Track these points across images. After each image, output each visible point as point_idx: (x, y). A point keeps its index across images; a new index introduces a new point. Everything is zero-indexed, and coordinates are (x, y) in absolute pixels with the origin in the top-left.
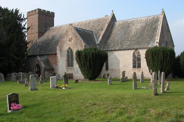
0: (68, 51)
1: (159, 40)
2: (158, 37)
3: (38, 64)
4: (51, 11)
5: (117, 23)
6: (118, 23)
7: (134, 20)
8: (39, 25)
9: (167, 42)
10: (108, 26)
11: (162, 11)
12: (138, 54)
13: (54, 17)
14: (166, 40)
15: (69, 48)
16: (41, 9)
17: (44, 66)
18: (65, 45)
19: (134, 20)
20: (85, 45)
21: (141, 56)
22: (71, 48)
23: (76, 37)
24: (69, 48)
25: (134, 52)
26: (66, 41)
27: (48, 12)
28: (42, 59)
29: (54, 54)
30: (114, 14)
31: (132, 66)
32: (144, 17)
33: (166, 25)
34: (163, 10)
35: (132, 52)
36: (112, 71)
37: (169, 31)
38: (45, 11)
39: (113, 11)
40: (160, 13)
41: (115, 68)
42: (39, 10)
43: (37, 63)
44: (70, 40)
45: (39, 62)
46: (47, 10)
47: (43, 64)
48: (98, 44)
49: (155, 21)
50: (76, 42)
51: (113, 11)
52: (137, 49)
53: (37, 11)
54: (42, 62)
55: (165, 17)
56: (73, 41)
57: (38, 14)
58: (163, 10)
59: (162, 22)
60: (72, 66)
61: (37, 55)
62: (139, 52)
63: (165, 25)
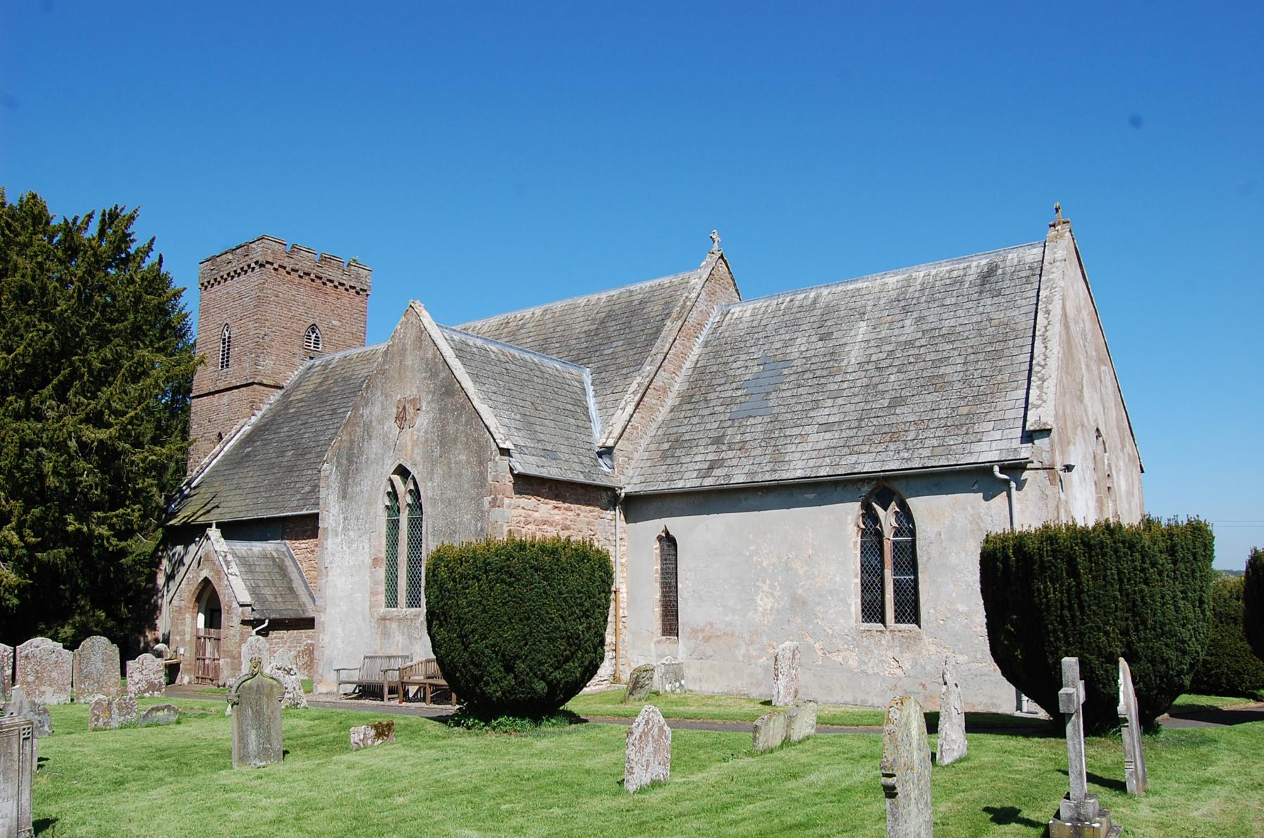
15: (403, 472)
26: (381, 421)
35: (851, 512)
36: (707, 639)
52: (882, 490)
54: (234, 569)
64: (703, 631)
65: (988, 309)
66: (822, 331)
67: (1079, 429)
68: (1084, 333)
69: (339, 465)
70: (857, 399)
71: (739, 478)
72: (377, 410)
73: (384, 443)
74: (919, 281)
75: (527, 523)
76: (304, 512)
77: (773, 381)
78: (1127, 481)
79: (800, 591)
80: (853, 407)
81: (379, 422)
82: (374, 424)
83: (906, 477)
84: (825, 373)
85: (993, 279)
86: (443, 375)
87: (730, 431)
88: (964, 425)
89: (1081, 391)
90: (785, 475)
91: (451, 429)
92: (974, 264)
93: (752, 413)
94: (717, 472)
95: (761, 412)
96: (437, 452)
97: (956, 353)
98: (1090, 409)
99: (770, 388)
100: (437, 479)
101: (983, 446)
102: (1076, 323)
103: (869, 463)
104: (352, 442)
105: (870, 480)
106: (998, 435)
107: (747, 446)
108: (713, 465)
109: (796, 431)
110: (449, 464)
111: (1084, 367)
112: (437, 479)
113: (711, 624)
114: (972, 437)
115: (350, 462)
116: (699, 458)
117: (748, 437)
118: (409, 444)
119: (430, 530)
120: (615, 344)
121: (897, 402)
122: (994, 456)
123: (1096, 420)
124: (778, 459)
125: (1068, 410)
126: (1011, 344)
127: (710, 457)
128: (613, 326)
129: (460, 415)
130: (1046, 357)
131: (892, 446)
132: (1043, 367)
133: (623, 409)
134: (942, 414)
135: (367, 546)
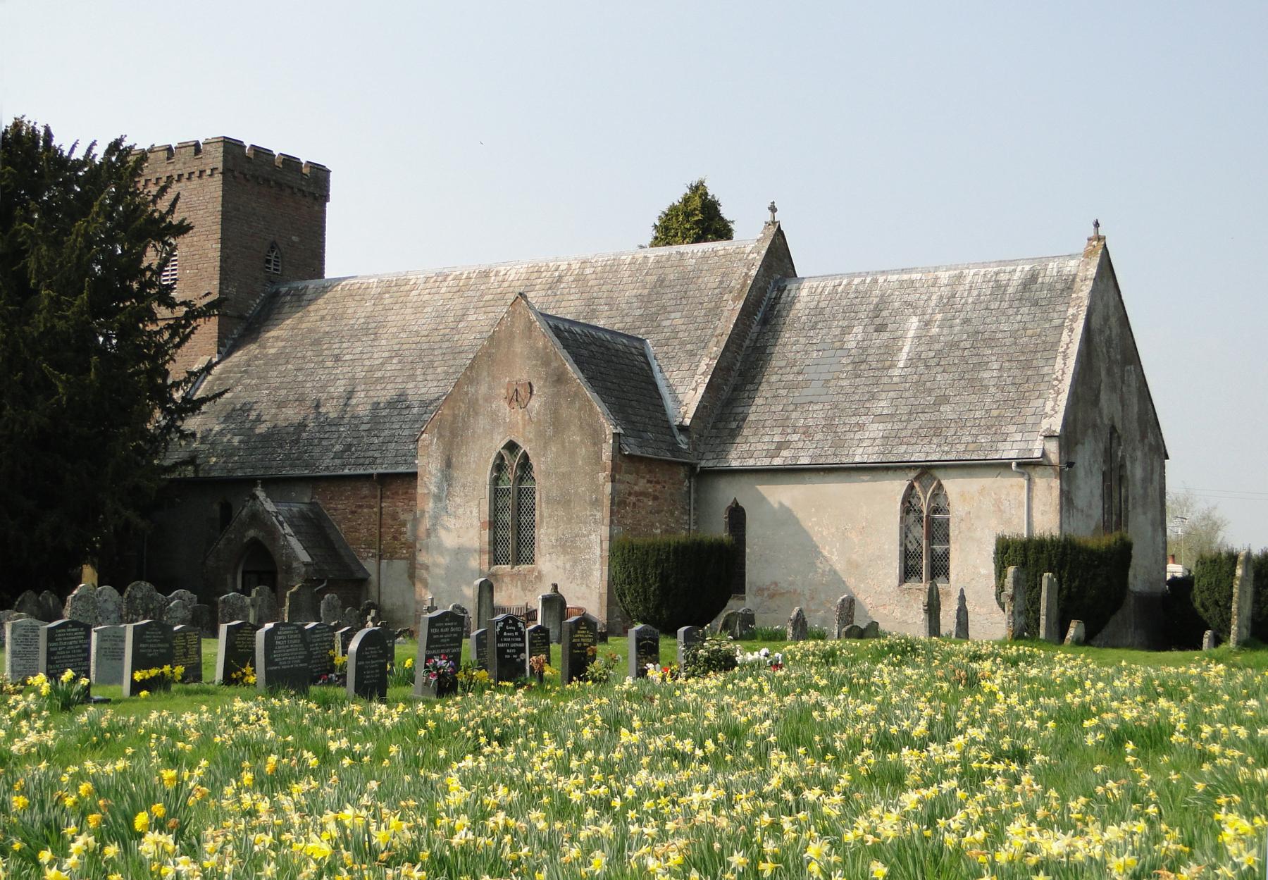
0: (499, 466)
1: (1060, 422)
2: (1055, 400)
3: (255, 542)
4: (305, 156)
5: (804, 296)
6: (806, 286)
7: (919, 276)
8: (224, 260)
9: (1113, 429)
10: (747, 313)
11: (1091, 232)
12: (934, 496)
13: (325, 198)
14: (1106, 421)
15: (512, 447)
16: (239, 145)
17: (304, 557)
18: (482, 422)
19: (914, 276)
20: (616, 436)
21: (951, 509)
22: (525, 447)
23: (560, 379)
24: (512, 447)
25: (911, 487)
26: (488, 399)
27: (291, 163)
28: (284, 508)
29: (371, 475)
30: (780, 233)
31: (894, 568)
32: (976, 265)
33: (1113, 321)
34: (1097, 224)
35: (896, 487)
36: (772, 596)
37: (1130, 355)
38: (268, 153)
39: (773, 209)
40: (1082, 245)
41: (791, 583)
42: (231, 147)
43: (251, 533)
44: (514, 398)
45: (272, 533)
46: (279, 147)
47: (295, 543)
48: (682, 429)
49: (1036, 292)
50: (555, 414)
51: (773, 209)
52: (925, 471)
53: (216, 158)
54: (288, 529)
55: (1106, 269)
56: (535, 404)
57: (218, 178)
58: (1097, 224)
59: (1084, 309)
60: (518, 561)
61: (250, 482)
62: (940, 486)
63: (1106, 319)
64: (768, 589)
65: (1026, 318)
66: (878, 321)
67: (1090, 431)
68: (1109, 341)
69: (441, 436)
70: (907, 394)
71: (804, 461)
72: (483, 389)
73: (493, 420)
74: (969, 279)
75: (630, 494)
76: (346, 471)
77: (833, 368)
78: (1144, 469)
79: (854, 557)
80: (904, 402)
81: (486, 400)
82: (481, 402)
83: (945, 467)
84: (879, 366)
85: (1034, 287)
86: (554, 364)
87: (794, 415)
88: (994, 427)
89: (1097, 396)
90: (844, 460)
91: (564, 412)
92: (1020, 268)
93: (814, 399)
94: (785, 453)
95: (822, 398)
96: (550, 432)
97: (994, 358)
98: (1105, 412)
99: (829, 376)
100: (550, 456)
101: (1007, 445)
102: (1101, 331)
103: (918, 454)
104: (455, 416)
105: (916, 467)
106: (1018, 437)
107: (811, 431)
108: (780, 446)
109: (854, 420)
110: (563, 443)
111: (1103, 373)
112: (550, 456)
113: (776, 584)
114: (999, 437)
115: (454, 434)
116: (766, 439)
117: (810, 422)
118: (521, 423)
119: (544, 499)
120: (673, 316)
121: (944, 400)
122: (1013, 454)
123: (1112, 419)
124: (839, 444)
125: (1080, 415)
126: (1039, 355)
127: (777, 439)
128: (668, 296)
129: (573, 402)
130: (1064, 373)
131: (935, 440)
132: (1060, 381)
133: (695, 389)
134: (978, 414)
135: (475, 511)
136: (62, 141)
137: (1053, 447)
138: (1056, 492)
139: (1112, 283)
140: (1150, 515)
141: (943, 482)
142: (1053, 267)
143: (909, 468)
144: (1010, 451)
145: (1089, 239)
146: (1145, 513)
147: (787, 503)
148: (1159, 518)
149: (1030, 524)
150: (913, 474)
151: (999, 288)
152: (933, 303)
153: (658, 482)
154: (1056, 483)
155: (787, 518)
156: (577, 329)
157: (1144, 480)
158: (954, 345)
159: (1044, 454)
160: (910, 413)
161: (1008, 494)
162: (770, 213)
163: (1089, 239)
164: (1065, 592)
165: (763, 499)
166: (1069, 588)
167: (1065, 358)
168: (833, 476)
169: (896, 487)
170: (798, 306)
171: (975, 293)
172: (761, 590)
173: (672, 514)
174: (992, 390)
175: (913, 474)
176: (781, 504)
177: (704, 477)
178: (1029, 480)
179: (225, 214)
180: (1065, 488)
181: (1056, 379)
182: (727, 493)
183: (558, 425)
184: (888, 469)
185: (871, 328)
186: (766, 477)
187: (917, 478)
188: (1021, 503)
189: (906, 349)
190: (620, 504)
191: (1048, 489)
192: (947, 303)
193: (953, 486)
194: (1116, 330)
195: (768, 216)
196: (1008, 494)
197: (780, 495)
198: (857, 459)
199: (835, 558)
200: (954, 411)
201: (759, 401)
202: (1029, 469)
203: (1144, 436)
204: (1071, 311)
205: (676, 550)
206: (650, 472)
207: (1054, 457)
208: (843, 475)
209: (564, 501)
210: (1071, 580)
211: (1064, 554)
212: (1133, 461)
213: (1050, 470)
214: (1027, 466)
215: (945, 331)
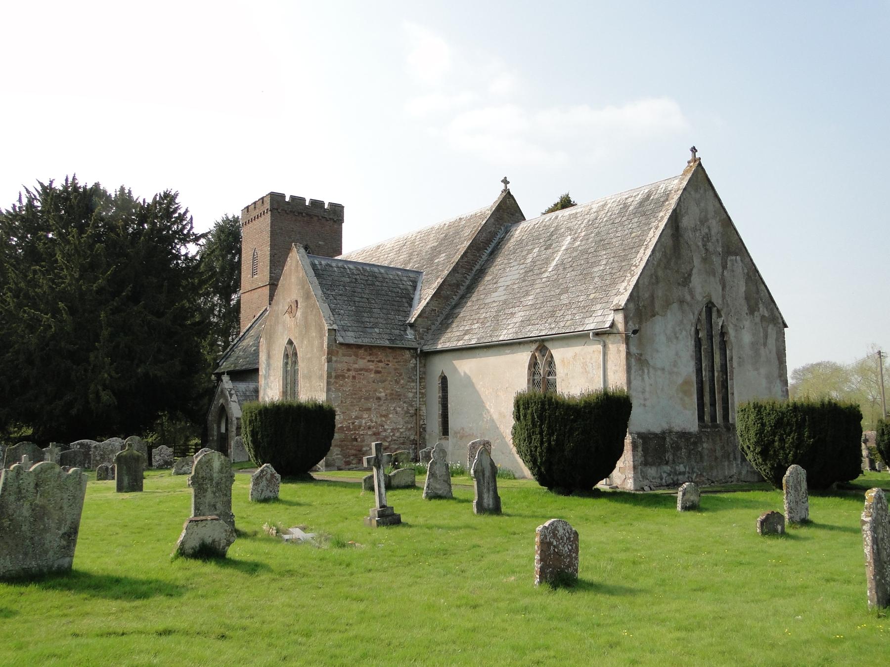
18: (280, 328)
25: (534, 357)
34: (694, 150)
38: (321, 204)
39: (505, 181)
42: (276, 198)
46: (309, 196)
52: (542, 345)
57: (269, 213)
75: (349, 370)
90: (494, 339)
103: (534, 332)
105: (536, 341)
121: (566, 290)
122: (592, 327)
136: (135, 196)
137: (620, 318)
138: (623, 354)
139: (711, 193)
140: (763, 371)
141: (552, 351)
142: (663, 186)
143: (531, 342)
144: (591, 325)
145: (689, 162)
146: (757, 369)
147: (468, 372)
148: (776, 372)
149: (605, 381)
150: (534, 347)
151: (626, 206)
152: (582, 226)
153: (380, 361)
154: (623, 348)
155: (468, 383)
156: (351, 266)
157: (754, 344)
158: (585, 252)
159: (613, 325)
160: (543, 303)
161: (591, 359)
162: (503, 185)
163: (689, 162)
164: (546, 444)
165: (455, 370)
166: (549, 441)
167: (646, 249)
168: (491, 351)
169: (524, 357)
170: (512, 240)
171: (609, 214)
172: (456, 433)
173: (397, 382)
174: (596, 279)
175: (534, 347)
176: (465, 373)
177: (426, 356)
178: (605, 346)
179: (271, 232)
180: (634, 350)
181: (635, 266)
182: (439, 366)
183: (307, 326)
184: (520, 343)
185: (543, 248)
186: (458, 354)
187: (537, 349)
188: (599, 364)
189: (557, 259)
190: (337, 377)
191: (617, 351)
192: (591, 224)
193: (559, 353)
194: (715, 226)
195: (502, 186)
196: (591, 359)
197: (466, 366)
198: (501, 339)
199: (492, 411)
200: (568, 298)
201: (469, 304)
202: (604, 337)
203: (752, 310)
204: (661, 214)
205: (260, 412)
206: (370, 354)
207: (621, 326)
208: (495, 350)
209: (308, 377)
210: (550, 434)
211: (543, 409)
212: (738, 329)
213: (618, 337)
214: (599, 334)
215: (583, 243)
